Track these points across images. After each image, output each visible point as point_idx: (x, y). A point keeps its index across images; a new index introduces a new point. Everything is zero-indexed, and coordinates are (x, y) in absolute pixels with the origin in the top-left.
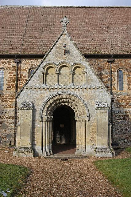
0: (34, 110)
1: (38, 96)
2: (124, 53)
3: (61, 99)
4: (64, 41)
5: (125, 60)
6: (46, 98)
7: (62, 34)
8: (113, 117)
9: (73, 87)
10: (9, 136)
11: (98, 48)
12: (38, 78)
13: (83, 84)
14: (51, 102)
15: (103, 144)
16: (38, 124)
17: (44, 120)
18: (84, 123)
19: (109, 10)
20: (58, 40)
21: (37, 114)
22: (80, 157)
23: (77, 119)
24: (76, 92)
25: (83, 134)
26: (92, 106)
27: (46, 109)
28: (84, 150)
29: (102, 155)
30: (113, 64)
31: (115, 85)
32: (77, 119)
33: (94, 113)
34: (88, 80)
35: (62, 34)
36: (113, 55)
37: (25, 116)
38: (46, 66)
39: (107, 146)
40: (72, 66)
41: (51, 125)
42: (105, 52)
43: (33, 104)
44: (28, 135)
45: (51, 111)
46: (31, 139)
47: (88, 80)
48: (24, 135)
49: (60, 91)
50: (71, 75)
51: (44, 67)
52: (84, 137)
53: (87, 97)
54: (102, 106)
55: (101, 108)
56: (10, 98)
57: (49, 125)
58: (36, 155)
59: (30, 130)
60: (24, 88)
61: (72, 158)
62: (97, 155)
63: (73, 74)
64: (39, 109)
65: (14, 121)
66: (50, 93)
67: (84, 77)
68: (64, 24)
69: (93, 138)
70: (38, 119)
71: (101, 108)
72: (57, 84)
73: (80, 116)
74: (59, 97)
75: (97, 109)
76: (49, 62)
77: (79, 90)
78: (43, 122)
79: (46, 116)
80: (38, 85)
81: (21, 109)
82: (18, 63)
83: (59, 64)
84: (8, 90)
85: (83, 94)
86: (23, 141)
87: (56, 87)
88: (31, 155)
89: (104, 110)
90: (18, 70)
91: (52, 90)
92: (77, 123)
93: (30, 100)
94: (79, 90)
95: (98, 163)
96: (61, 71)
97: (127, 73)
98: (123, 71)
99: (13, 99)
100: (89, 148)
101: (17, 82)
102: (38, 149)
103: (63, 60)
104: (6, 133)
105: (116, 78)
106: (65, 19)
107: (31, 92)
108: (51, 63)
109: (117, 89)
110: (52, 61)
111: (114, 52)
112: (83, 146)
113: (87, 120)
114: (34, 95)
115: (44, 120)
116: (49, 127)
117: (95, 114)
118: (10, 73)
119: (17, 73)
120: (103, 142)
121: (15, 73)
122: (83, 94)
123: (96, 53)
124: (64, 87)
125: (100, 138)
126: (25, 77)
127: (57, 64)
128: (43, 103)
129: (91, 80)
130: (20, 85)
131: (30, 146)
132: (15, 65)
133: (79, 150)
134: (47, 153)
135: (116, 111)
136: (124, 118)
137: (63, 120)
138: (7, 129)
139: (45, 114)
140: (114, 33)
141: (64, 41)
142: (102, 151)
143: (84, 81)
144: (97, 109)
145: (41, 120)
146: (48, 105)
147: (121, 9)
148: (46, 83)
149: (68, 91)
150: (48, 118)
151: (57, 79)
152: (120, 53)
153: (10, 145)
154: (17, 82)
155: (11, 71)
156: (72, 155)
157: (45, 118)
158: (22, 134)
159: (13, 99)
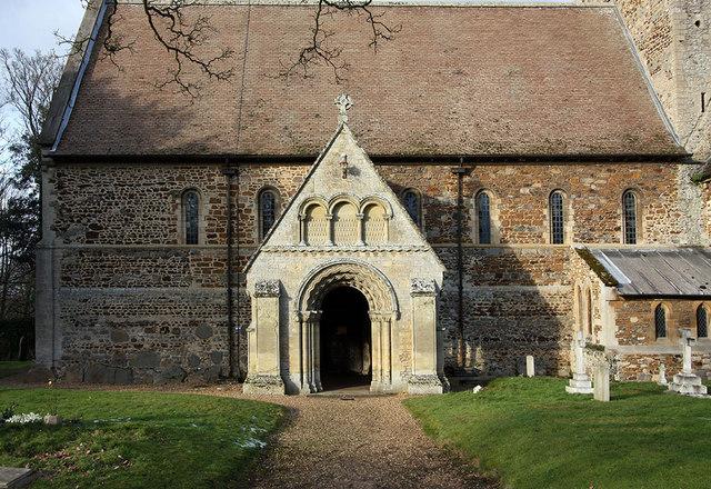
0: (283, 297)
1: (291, 269)
2: (492, 151)
3: (339, 273)
4: (342, 148)
5: (494, 168)
6: (306, 274)
7: (339, 133)
8: (465, 307)
9: (363, 248)
10: (216, 357)
11: (427, 136)
12: (289, 229)
13: (383, 242)
14: (317, 280)
15: (426, 368)
16: (293, 328)
17: (305, 318)
18: (386, 324)
19: (467, 14)
20: (330, 145)
21: (292, 306)
22: (379, 394)
23: (374, 316)
24: (371, 259)
25: (386, 348)
26: (404, 289)
27: (307, 297)
28: (387, 380)
29: (422, 390)
30: (466, 179)
31: (468, 229)
32: (373, 316)
33: (406, 304)
34: (394, 233)
35: (339, 133)
36: (464, 159)
37: (264, 313)
38: (305, 202)
39: (434, 373)
40: (362, 203)
41: (318, 330)
42: (446, 146)
43: (281, 285)
44: (272, 351)
45: (320, 293)
46: (273, 356)
47: (394, 233)
48: (263, 351)
49: (336, 258)
50: (359, 222)
51: (302, 207)
52: (386, 353)
53: (393, 270)
54: (424, 290)
55: (421, 293)
56: (216, 264)
57: (316, 329)
58: (290, 390)
59: (276, 339)
60: (260, 252)
61: (363, 396)
62: (412, 389)
63: (364, 221)
64: (293, 294)
65: (226, 318)
66: (313, 263)
67: (386, 228)
68: (343, 108)
69: (405, 357)
70: (293, 318)
71: (421, 293)
72: (328, 242)
73: (380, 308)
74: (333, 270)
75: (414, 294)
76: (312, 195)
77: (376, 255)
78: (301, 323)
79: (308, 310)
80: (288, 244)
81: (257, 295)
82: (231, 176)
83: (333, 200)
84: (211, 242)
85: (385, 263)
86: (261, 361)
87: (328, 249)
88: (280, 390)
89: (427, 299)
90: (231, 194)
91: (318, 255)
92: (374, 327)
93: (273, 277)
94: (376, 255)
95: (410, 403)
96: (339, 214)
97: (499, 201)
98: (491, 195)
99: (223, 265)
100: (396, 377)
101: (231, 223)
102: (295, 377)
103: (341, 191)
104: (208, 349)
105: (472, 211)
106: (344, 97)
107: (276, 259)
108: (314, 198)
109: (474, 241)
110: (317, 192)
111: (468, 150)
112: (386, 372)
113: (394, 318)
114: (283, 265)
115: (305, 318)
116: (307, 334)
117: (410, 305)
118: (212, 201)
119: (230, 200)
120: (426, 364)
121: (224, 201)
122: (385, 263)
123: (423, 150)
124: (344, 248)
125: (419, 355)
126: (249, 211)
127: (329, 198)
128: (300, 283)
129: (401, 233)
130: (238, 230)
131: (276, 373)
132: (224, 181)
133: (375, 384)
134: (311, 387)
135: (471, 296)
136: (492, 311)
137: (341, 318)
138: (211, 339)
139: (305, 306)
140: (472, 91)
141: (342, 148)
142: (423, 381)
143: (386, 235)
144: (414, 294)
145: (297, 319)
146: (311, 288)
147: (501, 13)
148: (306, 240)
149: (352, 258)
150: (312, 314)
151: (328, 231)
152: (481, 152)
153: (220, 376)
154: (231, 223)
155: (214, 195)
156: (365, 392)
157: (306, 314)
158: (262, 348)
159: (223, 265)
